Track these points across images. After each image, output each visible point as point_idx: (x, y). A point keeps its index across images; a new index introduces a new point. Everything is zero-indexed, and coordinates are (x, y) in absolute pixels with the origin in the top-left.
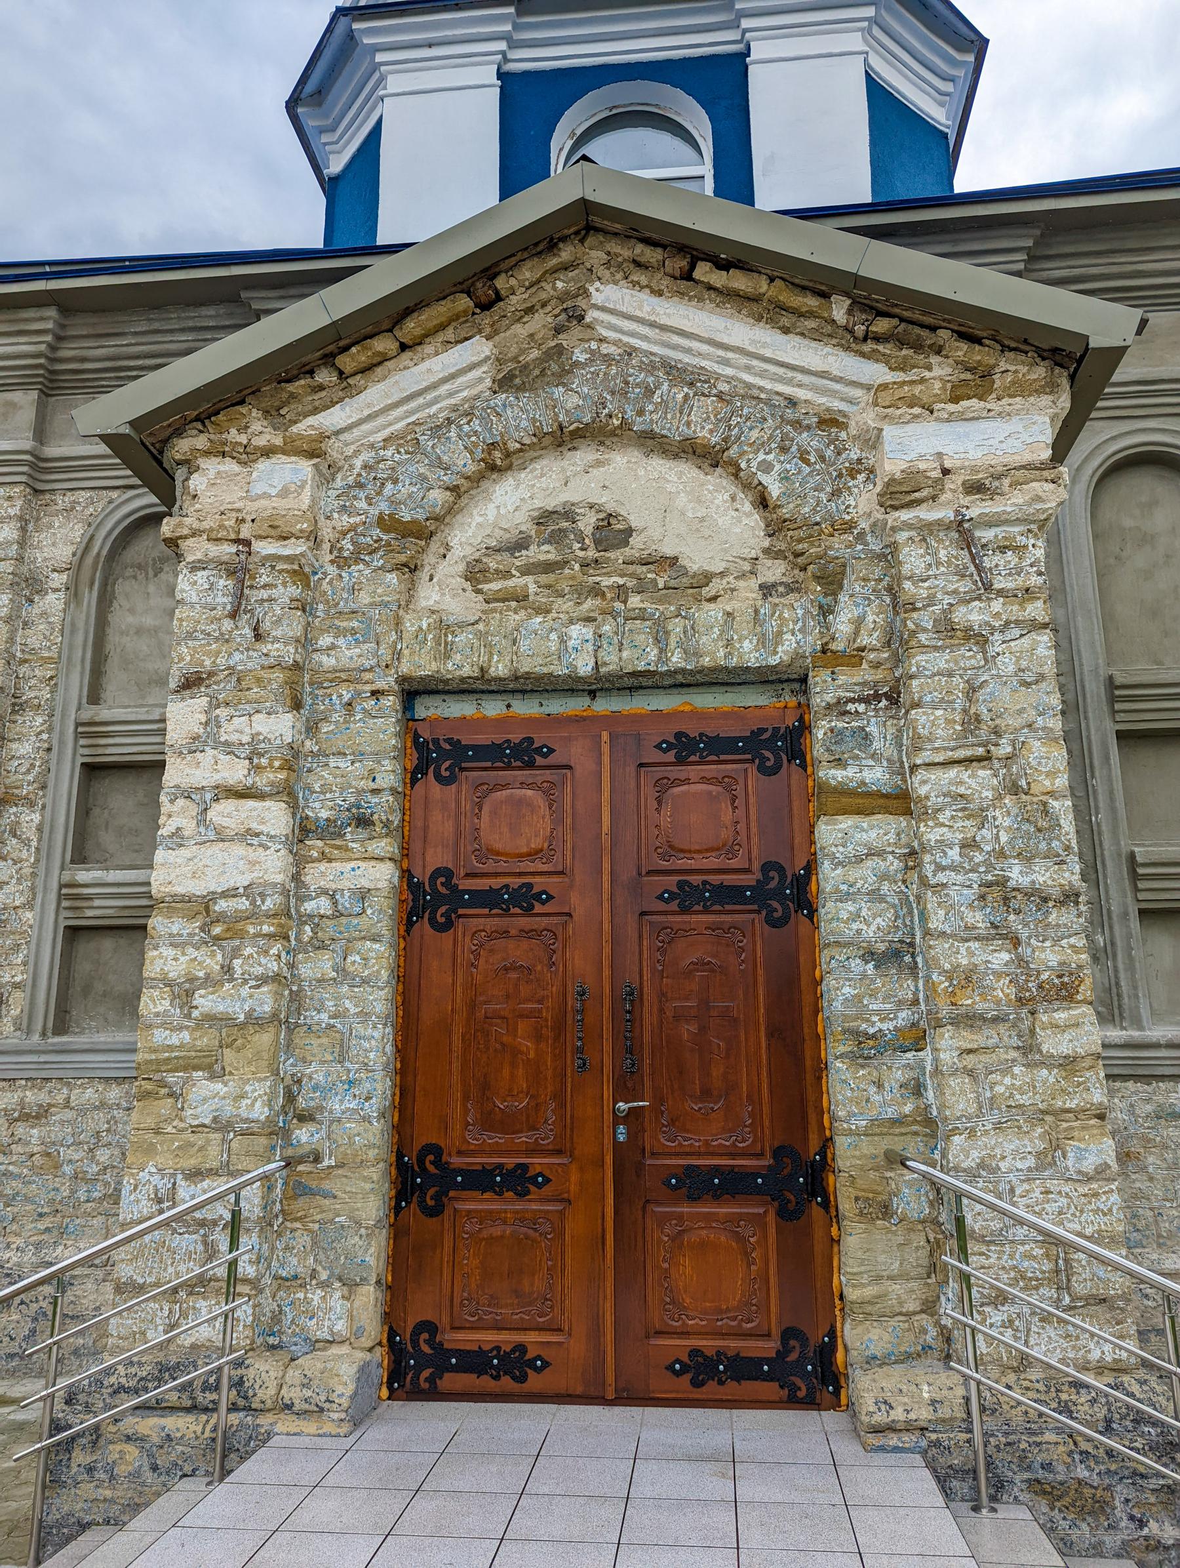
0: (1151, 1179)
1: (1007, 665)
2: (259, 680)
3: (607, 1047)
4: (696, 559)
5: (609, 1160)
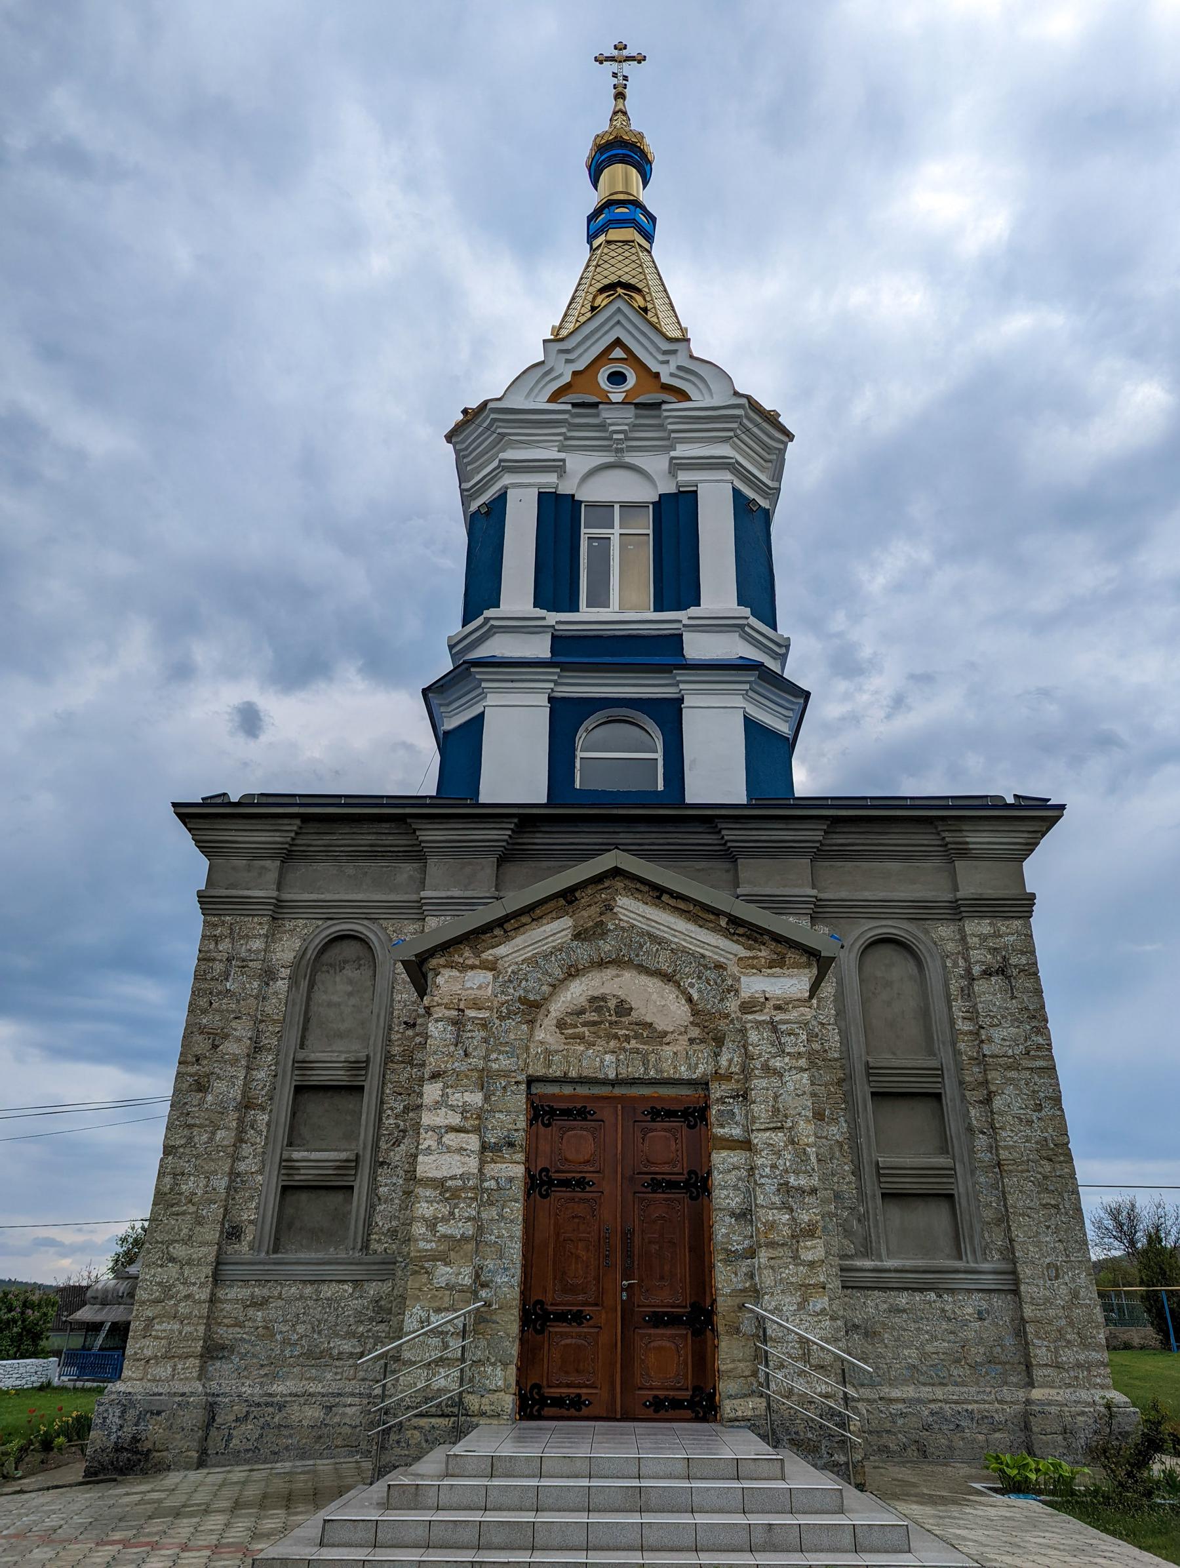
0: (886, 1347)
1: (790, 1086)
2: (467, 1076)
3: (619, 1254)
4: (661, 1025)
5: (619, 1308)
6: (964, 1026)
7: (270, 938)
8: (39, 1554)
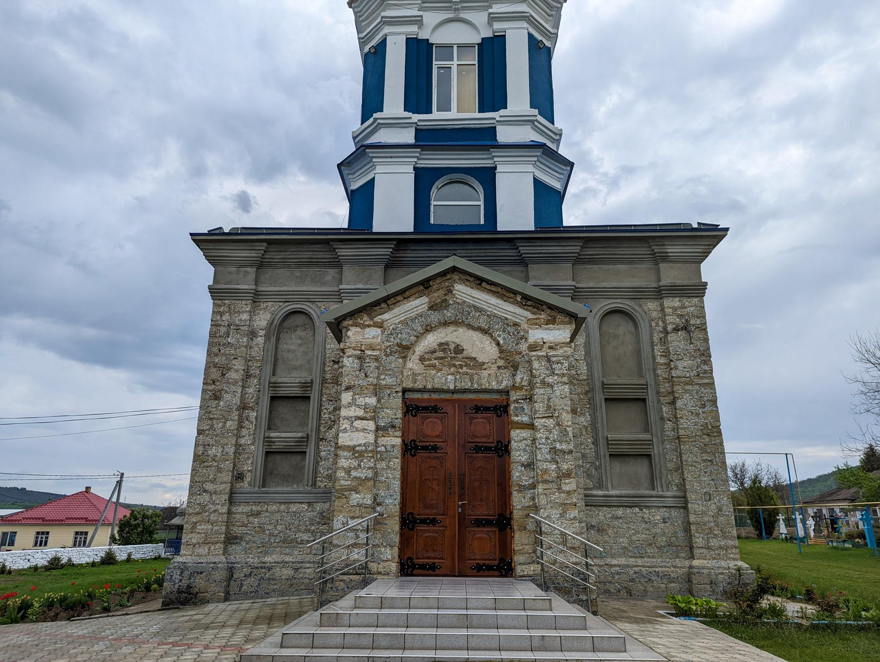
1: (558, 393)
6: (660, 360)
7: (252, 313)
8: (125, 650)
